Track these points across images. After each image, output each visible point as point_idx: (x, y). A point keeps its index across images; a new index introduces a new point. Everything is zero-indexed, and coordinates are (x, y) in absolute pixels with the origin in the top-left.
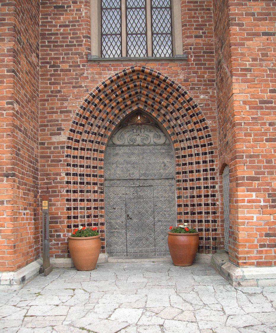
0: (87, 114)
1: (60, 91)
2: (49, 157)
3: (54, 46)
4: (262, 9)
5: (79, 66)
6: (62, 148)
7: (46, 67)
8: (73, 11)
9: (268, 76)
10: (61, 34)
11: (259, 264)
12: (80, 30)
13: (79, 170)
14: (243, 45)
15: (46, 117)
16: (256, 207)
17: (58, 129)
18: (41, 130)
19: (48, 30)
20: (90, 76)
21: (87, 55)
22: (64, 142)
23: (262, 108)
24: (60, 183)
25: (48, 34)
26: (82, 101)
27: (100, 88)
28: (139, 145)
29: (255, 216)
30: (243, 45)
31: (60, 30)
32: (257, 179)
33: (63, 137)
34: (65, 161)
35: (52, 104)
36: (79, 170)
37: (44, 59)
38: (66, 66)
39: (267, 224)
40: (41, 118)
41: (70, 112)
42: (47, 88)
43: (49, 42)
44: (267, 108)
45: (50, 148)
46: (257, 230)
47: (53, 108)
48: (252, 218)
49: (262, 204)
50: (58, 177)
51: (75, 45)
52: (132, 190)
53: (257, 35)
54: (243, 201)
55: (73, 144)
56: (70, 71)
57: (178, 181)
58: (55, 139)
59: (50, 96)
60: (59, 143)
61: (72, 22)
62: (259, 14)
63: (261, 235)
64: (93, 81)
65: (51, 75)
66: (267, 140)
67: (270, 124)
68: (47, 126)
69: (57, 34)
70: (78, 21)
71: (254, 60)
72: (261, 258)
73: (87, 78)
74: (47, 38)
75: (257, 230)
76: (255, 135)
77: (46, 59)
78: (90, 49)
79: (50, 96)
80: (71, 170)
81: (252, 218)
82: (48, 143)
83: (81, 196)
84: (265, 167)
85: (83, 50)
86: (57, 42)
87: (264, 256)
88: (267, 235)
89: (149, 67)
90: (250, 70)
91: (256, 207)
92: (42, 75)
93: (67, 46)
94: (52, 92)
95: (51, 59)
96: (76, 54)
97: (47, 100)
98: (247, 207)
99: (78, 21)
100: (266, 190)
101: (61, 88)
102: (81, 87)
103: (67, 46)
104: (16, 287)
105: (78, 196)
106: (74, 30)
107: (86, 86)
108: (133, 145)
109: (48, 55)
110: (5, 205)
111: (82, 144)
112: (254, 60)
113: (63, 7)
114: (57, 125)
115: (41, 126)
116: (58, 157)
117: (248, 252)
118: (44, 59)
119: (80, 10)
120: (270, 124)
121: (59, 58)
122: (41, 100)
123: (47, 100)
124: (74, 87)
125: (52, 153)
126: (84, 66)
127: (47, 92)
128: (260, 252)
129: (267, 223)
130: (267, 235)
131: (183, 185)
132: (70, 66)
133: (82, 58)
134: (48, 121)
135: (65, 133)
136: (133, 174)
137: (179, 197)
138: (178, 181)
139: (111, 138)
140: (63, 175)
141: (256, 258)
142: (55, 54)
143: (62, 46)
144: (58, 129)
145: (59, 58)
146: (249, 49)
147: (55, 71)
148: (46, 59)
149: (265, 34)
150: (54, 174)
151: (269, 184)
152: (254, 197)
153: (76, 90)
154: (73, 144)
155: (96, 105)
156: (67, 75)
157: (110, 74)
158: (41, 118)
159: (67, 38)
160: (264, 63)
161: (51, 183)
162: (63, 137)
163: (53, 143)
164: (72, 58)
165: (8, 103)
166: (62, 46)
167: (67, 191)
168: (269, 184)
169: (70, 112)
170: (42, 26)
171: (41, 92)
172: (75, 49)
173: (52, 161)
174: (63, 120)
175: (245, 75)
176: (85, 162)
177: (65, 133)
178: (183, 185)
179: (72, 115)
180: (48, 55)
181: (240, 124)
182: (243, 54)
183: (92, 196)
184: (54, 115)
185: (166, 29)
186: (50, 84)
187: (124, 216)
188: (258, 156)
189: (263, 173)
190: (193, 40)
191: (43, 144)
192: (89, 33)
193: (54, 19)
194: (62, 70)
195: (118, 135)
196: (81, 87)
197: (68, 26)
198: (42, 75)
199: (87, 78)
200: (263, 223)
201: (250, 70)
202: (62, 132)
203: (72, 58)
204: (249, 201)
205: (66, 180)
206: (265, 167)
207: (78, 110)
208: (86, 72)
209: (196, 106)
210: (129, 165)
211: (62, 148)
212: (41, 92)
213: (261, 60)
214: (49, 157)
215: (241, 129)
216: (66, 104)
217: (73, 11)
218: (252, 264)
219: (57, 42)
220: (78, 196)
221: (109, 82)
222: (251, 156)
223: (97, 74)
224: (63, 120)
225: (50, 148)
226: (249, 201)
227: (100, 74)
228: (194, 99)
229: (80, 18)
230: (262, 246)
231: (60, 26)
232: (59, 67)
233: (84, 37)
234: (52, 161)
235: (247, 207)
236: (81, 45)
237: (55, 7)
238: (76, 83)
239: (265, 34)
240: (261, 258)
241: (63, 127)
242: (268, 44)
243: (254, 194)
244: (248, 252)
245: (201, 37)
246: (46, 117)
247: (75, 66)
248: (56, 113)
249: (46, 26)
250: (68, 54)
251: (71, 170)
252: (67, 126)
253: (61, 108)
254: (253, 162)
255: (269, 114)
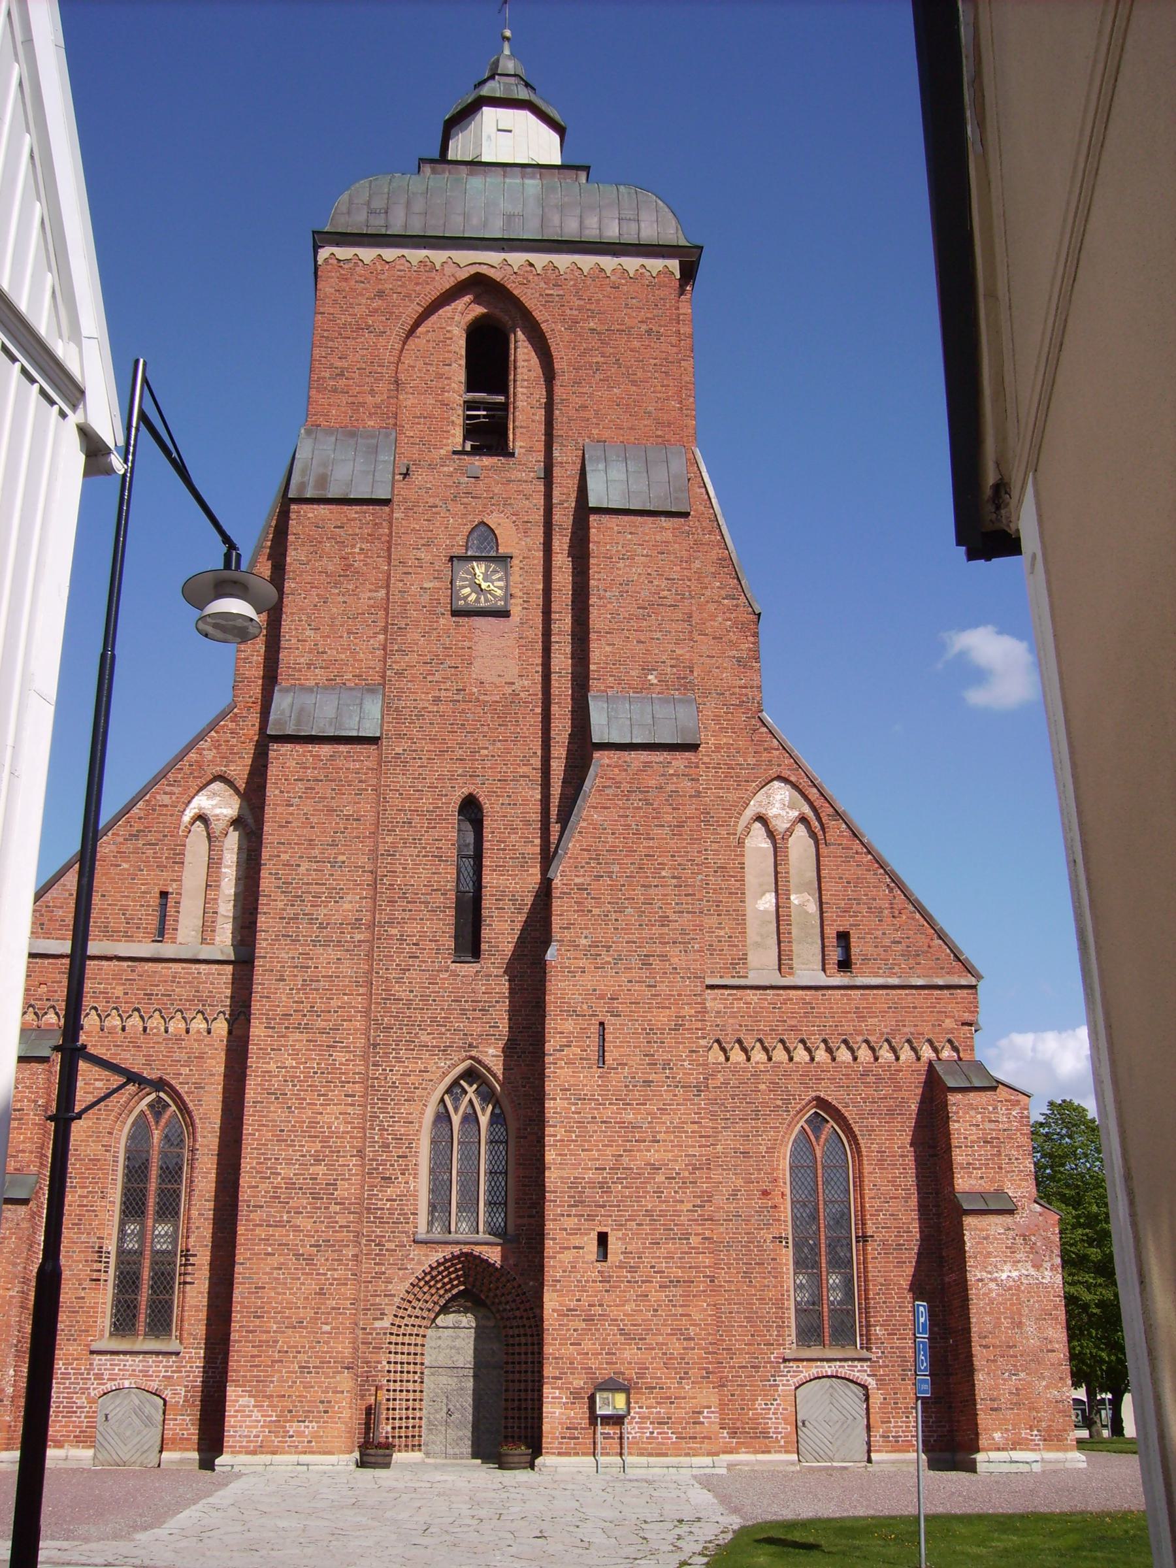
0: (411, 1297)
1: (384, 1273)
2: (371, 1343)
3: (380, 1222)
4: (575, 1224)
5: (405, 1246)
6: (385, 1334)
7: (371, 1245)
8: (401, 1183)
9: (575, 1286)
10: (388, 1209)
11: (560, 1454)
12: (407, 1205)
13: (399, 1358)
14: (555, 1257)
15: (369, 1301)
16: (559, 1403)
17: (381, 1314)
18: (364, 1314)
19: (374, 1204)
20: (416, 1258)
21: (414, 1234)
22: (387, 1328)
23: (568, 1315)
24: (381, 1371)
25: (374, 1209)
26: (407, 1285)
27: (427, 1271)
28: (464, 1328)
29: (558, 1411)
30: (555, 1257)
31: (385, 1204)
32: (561, 1378)
33: (386, 1323)
34: (387, 1348)
35: (375, 1286)
36: (399, 1358)
37: (368, 1236)
38: (392, 1246)
39: (568, 1418)
40: (364, 1300)
41: (394, 1296)
42: (371, 1268)
43: (374, 1217)
44: (572, 1315)
45: (371, 1334)
46: (559, 1423)
47: (376, 1291)
48: (555, 1413)
49: (564, 1400)
50: (379, 1366)
51: (402, 1223)
52: (456, 1379)
53: (568, 1248)
54: (548, 1397)
55: (395, 1330)
56: (396, 1251)
57: (506, 1372)
58: (378, 1324)
59: (374, 1277)
60: (381, 1329)
61: (399, 1196)
62: (571, 1229)
63: (562, 1429)
64: (420, 1263)
65: (376, 1255)
66: (571, 1344)
67: (574, 1330)
68: (370, 1309)
69: (383, 1209)
70: (406, 1196)
71: (564, 1271)
72: (562, 1448)
73: (413, 1259)
74: (372, 1213)
75: (559, 1423)
76: (561, 1339)
77: (371, 1236)
78: (416, 1227)
79: (374, 1277)
80: (392, 1357)
81: (555, 1413)
82: (371, 1329)
83: (401, 1386)
84: (568, 1368)
85: (409, 1228)
86: (383, 1218)
87: (564, 1446)
88: (568, 1428)
89: (477, 1250)
90: (560, 1281)
91: (559, 1403)
92: (366, 1254)
93: (393, 1223)
94: (376, 1273)
95: (377, 1236)
96: (402, 1232)
97: (371, 1282)
98: (551, 1403)
99: (406, 1196)
100: (569, 1388)
101: (386, 1269)
102: (406, 1269)
103: (393, 1223)
104: (353, 1467)
105: (398, 1386)
106: (402, 1205)
107: (412, 1269)
108: (458, 1328)
109: (373, 1232)
110: (345, 1394)
111: (405, 1330)
112: (564, 1271)
113: (391, 1178)
114: (380, 1309)
115: (364, 1310)
116: (381, 1344)
117: (550, 1443)
118: (368, 1236)
119: (407, 1183)
120: (574, 1330)
121: (384, 1237)
122: (365, 1282)
123: (371, 1282)
124: (399, 1269)
125: (374, 1339)
126: (410, 1246)
127: (371, 1273)
128: (561, 1443)
129: (568, 1418)
130: (568, 1428)
131: (511, 1377)
132: (396, 1246)
133: (409, 1237)
134: (371, 1305)
135: (388, 1318)
136: (457, 1361)
137: (506, 1390)
138: (506, 1372)
139: (434, 1320)
140: (384, 1363)
141: (557, 1448)
142: (381, 1232)
143: (388, 1223)
144: (381, 1314)
145: (384, 1237)
146: (560, 1262)
147: (380, 1250)
148: (371, 1236)
149: (575, 1248)
150: (375, 1362)
151: (571, 1383)
152: (557, 1395)
153: (401, 1272)
154: (395, 1330)
155: (421, 1288)
156: (392, 1256)
157: (438, 1255)
158: (364, 1300)
159: (394, 1214)
160: (573, 1275)
161: (371, 1372)
162: (386, 1323)
163: (375, 1329)
164: (398, 1237)
165: (351, 1304)
166: (388, 1223)
167: (388, 1381)
168: (571, 1383)
169: (394, 1296)
170: (367, 1199)
171: (365, 1273)
172: (402, 1227)
173: (374, 1348)
174: (386, 1304)
175: (556, 1286)
176: (406, 1349)
177: (388, 1318)
178: (511, 1377)
179: (397, 1300)
180: (373, 1232)
181: (548, 1330)
182: (555, 1267)
183: (411, 1386)
184: (378, 1298)
185: (500, 1199)
186: (375, 1264)
187: (445, 1410)
188: (562, 1358)
189: (566, 1373)
190: (525, 1221)
191: (365, 1329)
192: (417, 1209)
193: (381, 1191)
194: (387, 1250)
195: (442, 1316)
196: (406, 1269)
197: (395, 1200)
198: (366, 1254)
199: (413, 1259)
200: (564, 1417)
201: (560, 1281)
202: (385, 1317)
203: (398, 1237)
204: (553, 1398)
205: (387, 1368)
206: (568, 1368)
207: (403, 1294)
208: (412, 1253)
209: (525, 1293)
210: (453, 1351)
211: (385, 1334)
212: (365, 1273)
213: (570, 1272)
214: (371, 1343)
215: (548, 1334)
216: (390, 1287)
217: (401, 1183)
218: (553, 1454)
219: (383, 1218)
220: (398, 1386)
221: (436, 1264)
222: (556, 1358)
223: (424, 1255)
224: (386, 1304)
225: (371, 1334)
226: (553, 1398)
227: (427, 1255)
228: (523, 1286)
229: (407, 1191)
230: (563, 1438)
231: (387, 1200)
232: (384, 1246)
233: (412, 1214)
234: (374, 1348)
235: (551, 1403)
236: (408, 1223)
237: (382, 1178)
238: (402, 1265)
239: (575, 1248)
240: (562, 1448)
241: (386, 1312)
242: (577, 1257)
243: (557, 1391)
244: (550, 1443)
245: (534, 1217)
246: (369, 1301)
247: (401, 1246)
248: (380, 1296)
249: (371, 1199)
250: (394, 1232)
251: (392, 1357)
252: (390, 1310)
253: (385, 1291)
254: (558, 1363)
255: (574, 1321)
